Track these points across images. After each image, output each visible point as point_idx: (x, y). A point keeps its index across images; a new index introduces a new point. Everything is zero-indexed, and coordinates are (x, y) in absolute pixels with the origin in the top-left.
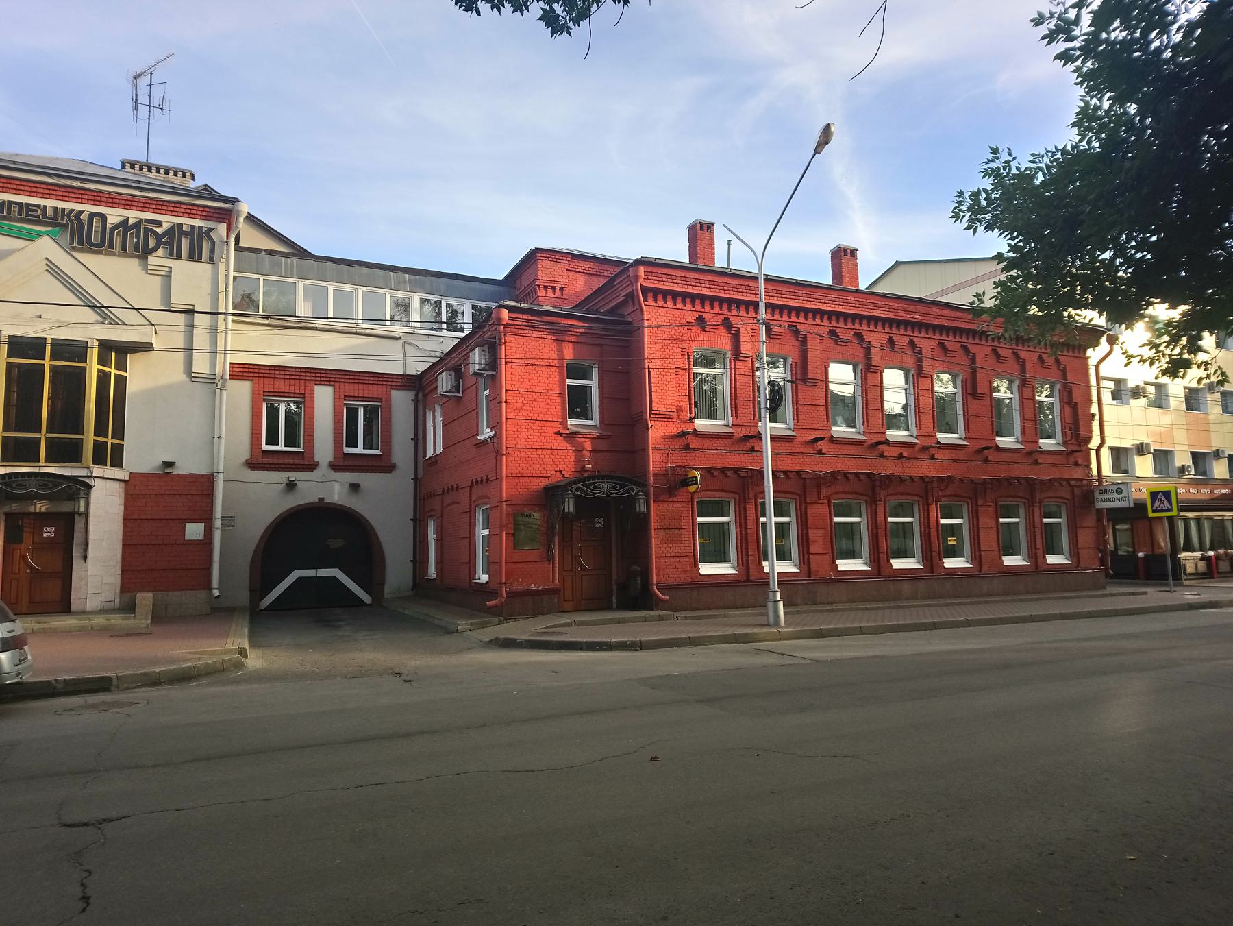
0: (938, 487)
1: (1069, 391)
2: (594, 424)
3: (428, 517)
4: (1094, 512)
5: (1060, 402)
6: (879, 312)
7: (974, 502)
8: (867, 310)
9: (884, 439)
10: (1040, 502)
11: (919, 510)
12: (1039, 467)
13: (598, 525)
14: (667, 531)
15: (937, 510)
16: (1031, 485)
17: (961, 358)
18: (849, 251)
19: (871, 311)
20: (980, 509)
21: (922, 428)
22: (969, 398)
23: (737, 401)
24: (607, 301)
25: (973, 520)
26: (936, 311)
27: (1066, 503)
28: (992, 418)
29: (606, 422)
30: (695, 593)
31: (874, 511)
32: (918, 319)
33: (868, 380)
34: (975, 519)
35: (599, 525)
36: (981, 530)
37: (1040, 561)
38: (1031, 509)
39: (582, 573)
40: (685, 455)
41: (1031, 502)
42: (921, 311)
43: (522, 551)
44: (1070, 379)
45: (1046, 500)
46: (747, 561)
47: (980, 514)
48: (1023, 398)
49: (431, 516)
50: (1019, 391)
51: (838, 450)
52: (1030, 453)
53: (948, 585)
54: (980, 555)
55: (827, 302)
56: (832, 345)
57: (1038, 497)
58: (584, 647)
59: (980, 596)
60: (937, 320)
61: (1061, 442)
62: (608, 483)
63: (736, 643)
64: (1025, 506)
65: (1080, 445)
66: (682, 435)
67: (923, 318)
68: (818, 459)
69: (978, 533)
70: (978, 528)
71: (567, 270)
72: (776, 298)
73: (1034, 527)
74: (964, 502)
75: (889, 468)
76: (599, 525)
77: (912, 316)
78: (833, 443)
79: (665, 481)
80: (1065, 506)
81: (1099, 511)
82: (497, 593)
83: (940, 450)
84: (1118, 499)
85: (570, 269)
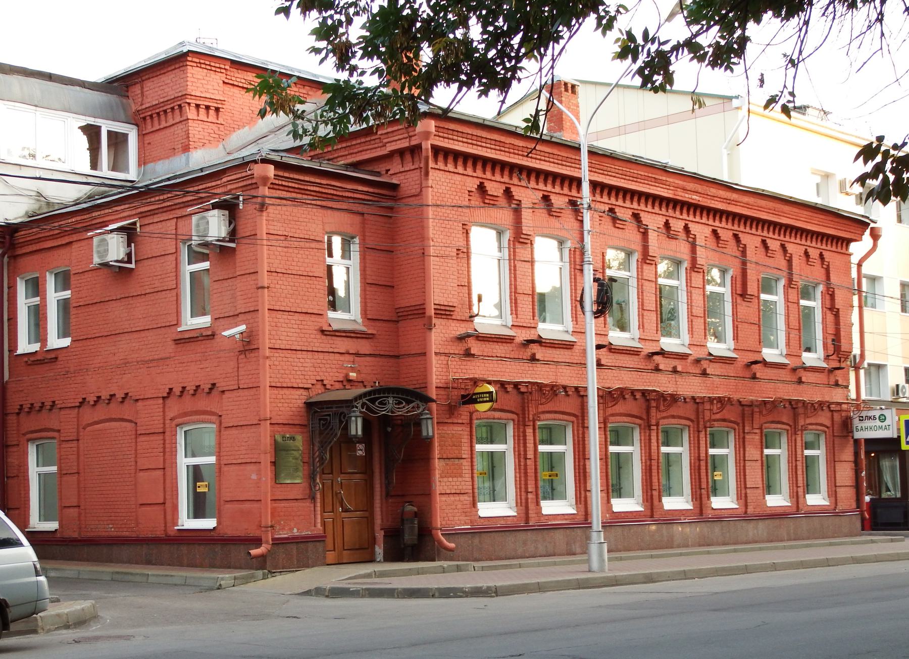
0: (804, 414)
1: (831, 295)
2: (353, 318)
3: (28, 440)
4: (852, 442)
5: (822, 307)
6: (659, 189)
7: (741, 428)
8: (648, 186)
9: (659, 349)
10: (657, 425)
11: (690, 437)
12: (802, 386)
13: (360, 453)
14: (447, 461)
15: (706, 437)
16: (794, 406)
17: (732, 248)
18: (570, 86)
19: (652, 187)
20: (747, 437)
21: (694, 336)
22: (739, 300)
23: (517, 295)
24: (352, 151)
25: (739, 451)
26: (713, 191)
27: (825, 432)
28: (799, 330)
29: (369, 317)
30: (476, 540)
31: (647, 438)
32: (696, 200)
33: (644, 274)
34: (742, 449)
35: (360, 452)
36: (748, 464)
37: (801, 500)
38: (793, 438)
39: (344, 515)
40: (464, 363)
41: (794, 430)
42: (700, 190)
43: (283, 485)
44: (834, 279)
45: (542, 416)
46: (527, 499)
47: (747, 443)
48: (788, 301)
49: (38, 435)
50: (784, 292)
51: (615, 361)
52: (794, 370)
53: (717, 528)
54: (746, 494)
55: (610, 173)
56: (609, 227)
57: (801, 422)
58: (437, 594)
59: (746, 543)
60: (713, 202)
61: (822, 356)
62: (394, 397)
63: (579, 588)
64: (788, 434)
65: (840, 361)
66: (461, 338)
67: (701, 199)
68: (527, 366)
69: (744, 466)
70: (745, 460)
71: (224, 82)
72: (560, 166)
73: (796, 461)
74: (731, 428)
75: (663, 384)
76: (360, 452)
77: (690, 196)
78: (611, 352)
79: (445, 397)
80: (824, 435)
81: (857, 442)
82: (261, 540)
83: (712, 364)
84: (881, 428)
85: (226, 81)
